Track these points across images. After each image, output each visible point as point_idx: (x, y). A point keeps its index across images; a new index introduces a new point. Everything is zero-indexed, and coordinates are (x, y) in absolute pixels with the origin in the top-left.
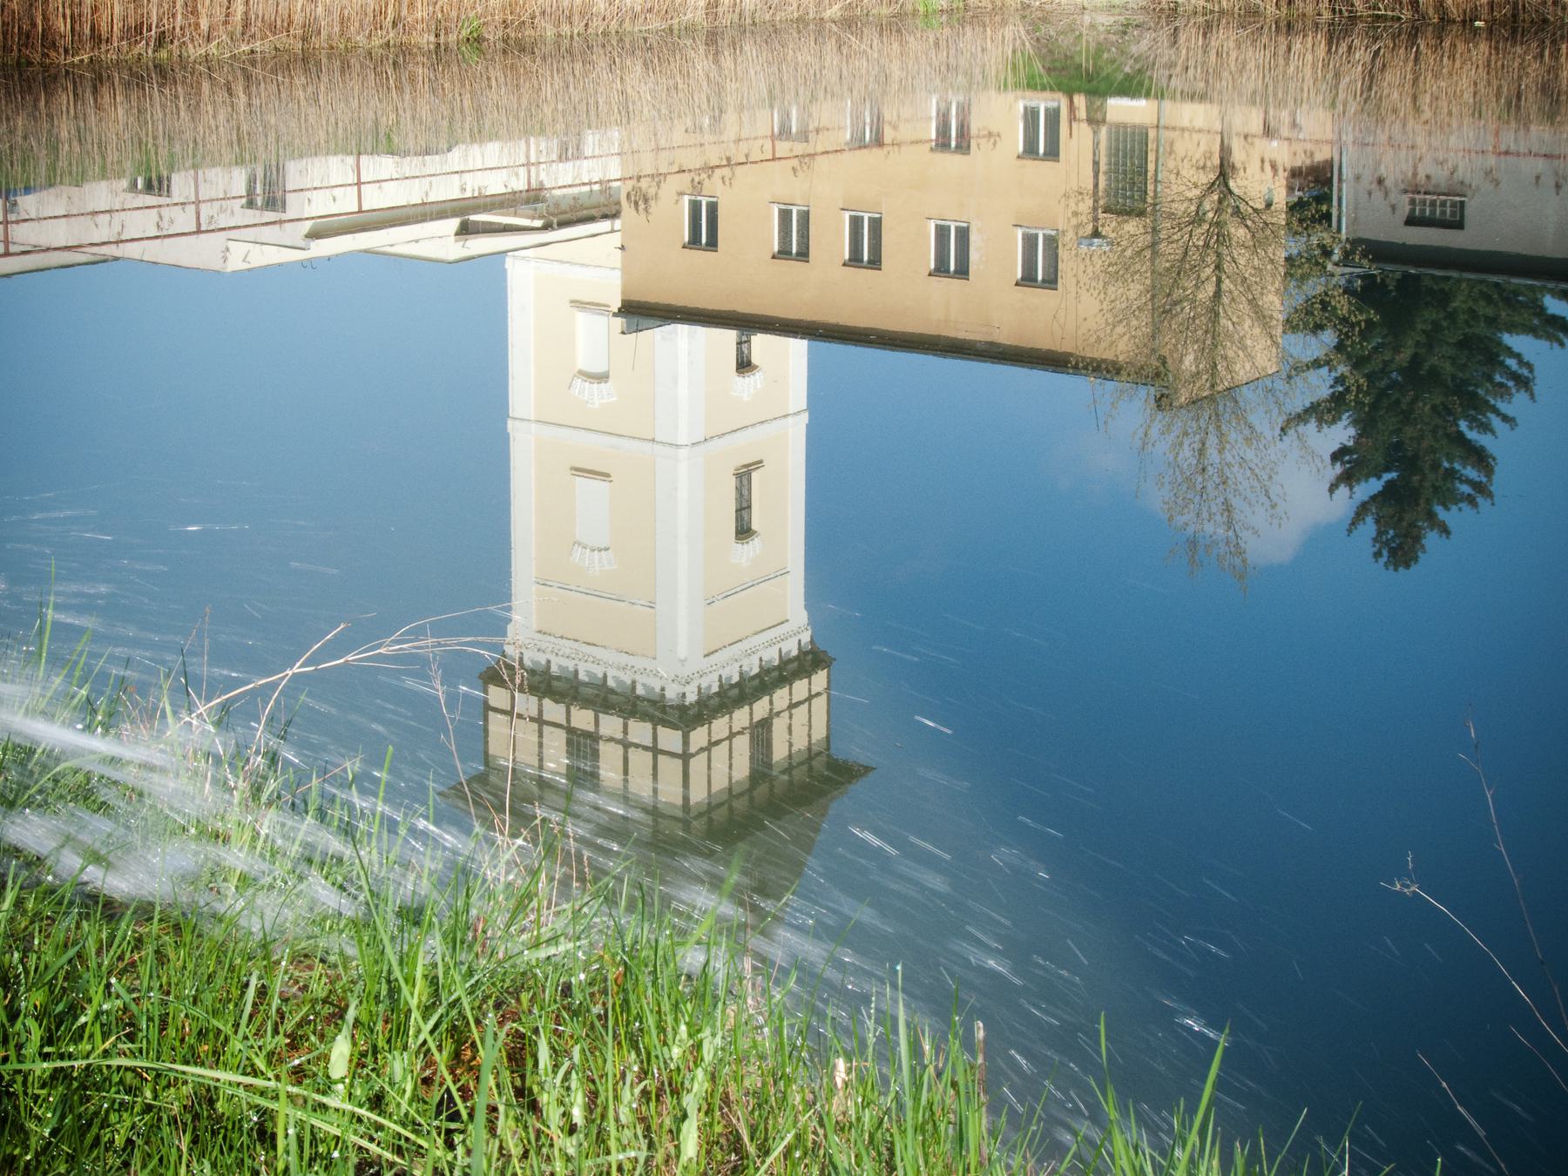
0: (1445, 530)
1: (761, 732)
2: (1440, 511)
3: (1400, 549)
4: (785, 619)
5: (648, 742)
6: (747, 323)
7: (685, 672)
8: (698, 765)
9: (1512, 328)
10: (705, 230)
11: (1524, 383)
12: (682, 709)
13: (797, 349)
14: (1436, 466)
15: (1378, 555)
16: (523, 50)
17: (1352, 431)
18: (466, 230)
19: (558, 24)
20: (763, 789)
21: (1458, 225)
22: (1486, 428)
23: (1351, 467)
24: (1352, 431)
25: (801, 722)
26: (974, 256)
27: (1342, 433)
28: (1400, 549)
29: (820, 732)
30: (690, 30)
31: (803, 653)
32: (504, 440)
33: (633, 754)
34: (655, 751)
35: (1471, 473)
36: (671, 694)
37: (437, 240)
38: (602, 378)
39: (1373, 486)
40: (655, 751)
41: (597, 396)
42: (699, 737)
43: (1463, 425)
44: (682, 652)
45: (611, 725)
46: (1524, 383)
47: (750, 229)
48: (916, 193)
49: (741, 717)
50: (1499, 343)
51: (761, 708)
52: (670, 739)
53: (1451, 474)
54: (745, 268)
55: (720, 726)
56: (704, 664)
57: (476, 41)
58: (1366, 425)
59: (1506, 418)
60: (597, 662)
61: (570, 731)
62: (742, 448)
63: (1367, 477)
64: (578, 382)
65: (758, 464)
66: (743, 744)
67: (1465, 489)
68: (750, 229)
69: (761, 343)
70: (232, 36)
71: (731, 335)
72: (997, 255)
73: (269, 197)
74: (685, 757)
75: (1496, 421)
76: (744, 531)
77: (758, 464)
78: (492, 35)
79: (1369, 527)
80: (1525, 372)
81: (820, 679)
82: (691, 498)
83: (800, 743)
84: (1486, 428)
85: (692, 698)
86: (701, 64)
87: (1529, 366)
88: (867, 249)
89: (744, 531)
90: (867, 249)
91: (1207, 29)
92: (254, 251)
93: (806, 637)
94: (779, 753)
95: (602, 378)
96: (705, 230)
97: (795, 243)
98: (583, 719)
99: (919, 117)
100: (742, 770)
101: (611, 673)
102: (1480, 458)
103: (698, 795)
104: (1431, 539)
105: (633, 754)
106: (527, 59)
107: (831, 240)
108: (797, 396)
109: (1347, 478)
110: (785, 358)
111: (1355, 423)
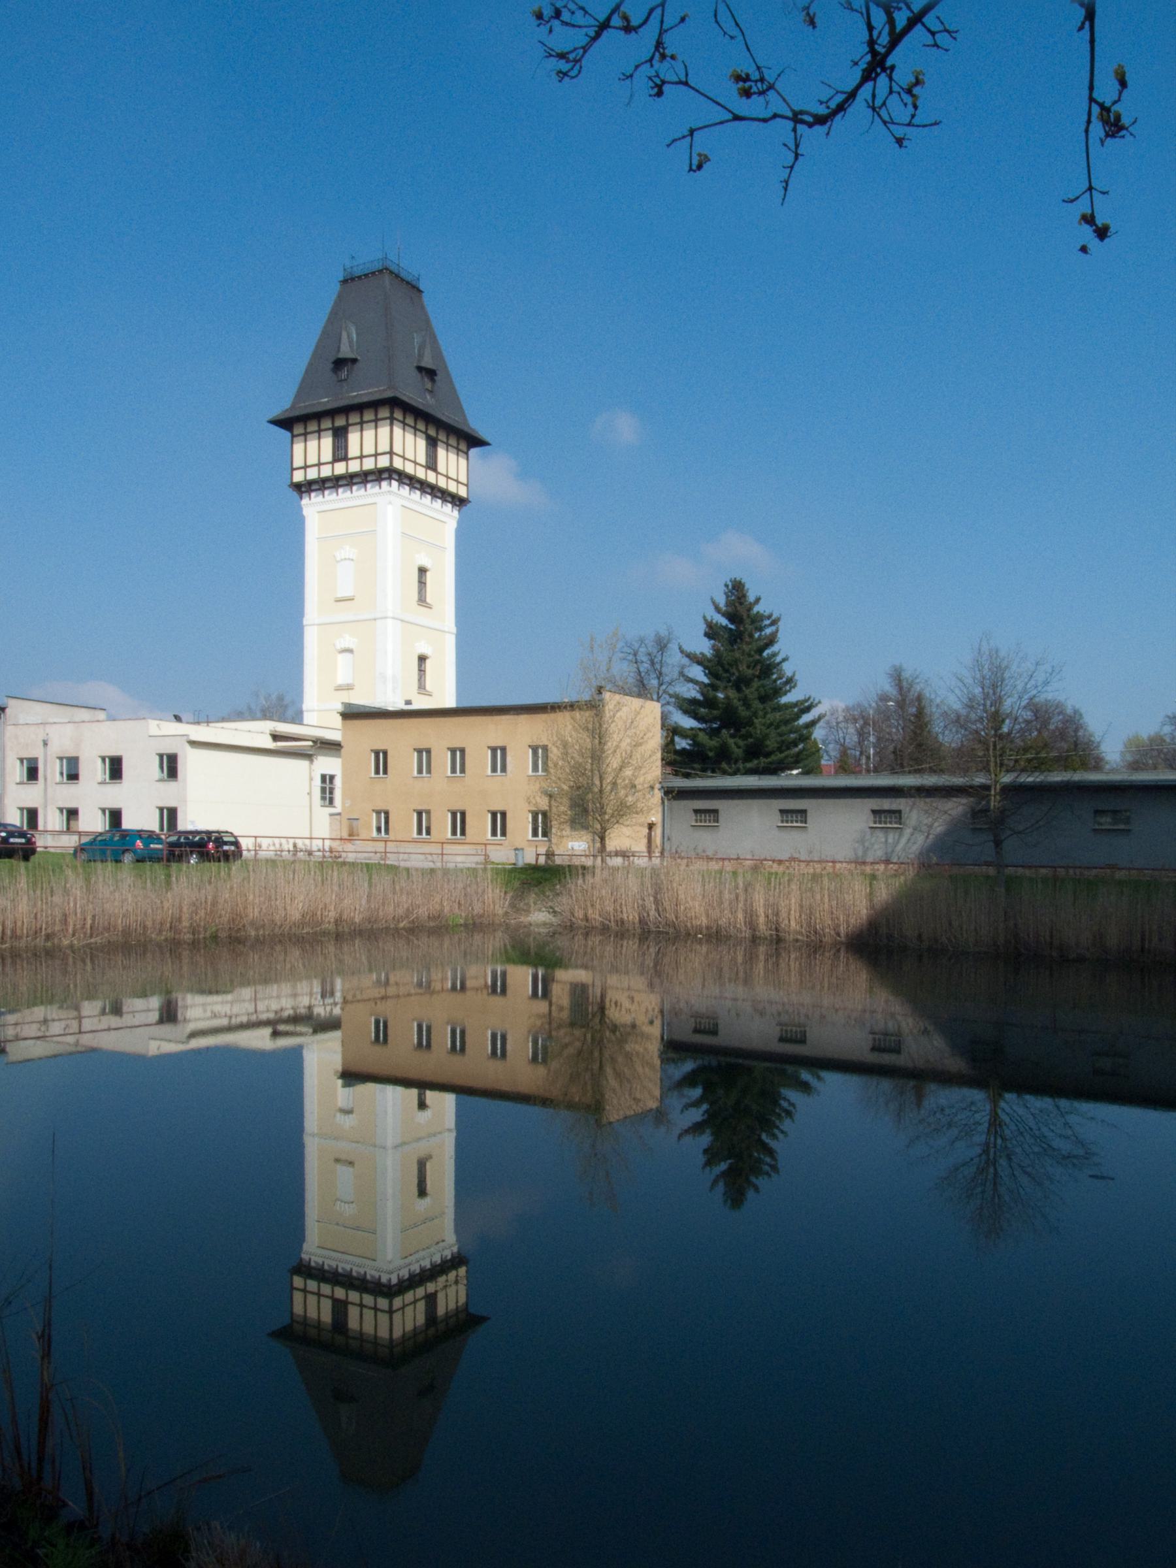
0: (757, 1189)
1: (431, 1299)
2: (753, 1179)
3: (736, 1198)
4: (445, 1238)
5: (316, 1290)
6: (422, 1085)
7: (391, 1267)
8: (397, 1317)
9: (784, 1086)
10: (382, 1034)
11: (789, 1113)
12: (389, 1286)
13: (450, 1099)
14: (751, 1156)
15: (725, 1201)
16: (240, 943)
17: (710, 1138)
18: (275, 1034)
19: (257, 929)
20: (431, 1331)
21: (898, 1051)
22: (774, 1137)
23: (712, 1157)
24: (710, 1138)
25: (452, 1294)
26: (509, 1047)
27: (705, 1139)
28: (736, 1198)
29: (462, 1299)
30: (325, 933)
31: (453, 1258)
32: (300, 1147)
33: (365, 1310)
34: (375, 1309)
35: (768, 1160)
36: (384, 1280)
37: (260, 1040)
38: (349, 1112)
39: (724, 1166)
40: (375, 1309)
41: (347, 1122)
42: (397, 1302)
43: (764, 1136)
44: (389, 1257)
45: (354, 1296)
46: (789, 1113)
47: (404, 1035)
48: (486, 1018)
49: (420, 1292)
50: (779, 1094)
51: (431, 1287)
52: (383, 1303)
53: (759, 1161)
54: (401, 1051)
55: (409, 1296)
56: (402, 1262)
57: (215, 938)
58: (716, 1135)
59: (782, 1132)
60: (347, 1262)
61: (332, 1297)
62: (422, 1148)
63: (720, 1161)
64: (338, 1114)
65: (430, 1157)
66: (421, 1306)
67: (766, 1168)
68: (404, 1035)
69: (429, 1095)
70: (85, 934)
71: (414, 1092)
72: (520, 1047)
73: (169, 1015)
74: (391, 1312)
75: (781, 1136)
76: (422, 1192)
77: (430, 1157)
78: (223, 935)
79: (721, 1186)
80: (791, 1108)
81: (462, 1271)
82: (394, 1175)
83: (452, 1306)
84: (774, 1137)
85: (394, 1281)
86: (331, 948)
87: (793, 1105)
88: (459, 1046)
89: (422, 1192)
90: (459, 1046)
91: (586, 935)
92: (162, 1043)
93: (455, 1249)
94: (441, 1311)
95: (349, 1112)
96: (382, 1034)
97: (425, 1043)
98: (340, 1293)
99: (443, 978)
100: (421, 1319)
101: (355, 1269)
102: (770, 1152)
103: (397, 1333)
104: (750, 1194)
105: (365, 1310)
106: (241, 946)
107: (443, 1039)
108: (450, 1120)
109: (709, 1163)
110: (445, 1104)
111: (712, 1134)
